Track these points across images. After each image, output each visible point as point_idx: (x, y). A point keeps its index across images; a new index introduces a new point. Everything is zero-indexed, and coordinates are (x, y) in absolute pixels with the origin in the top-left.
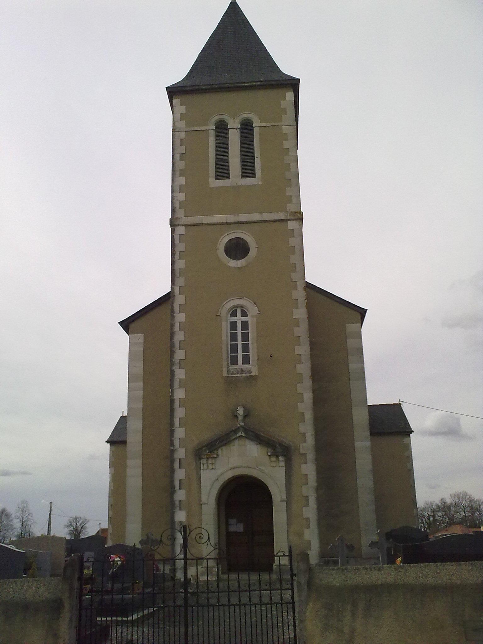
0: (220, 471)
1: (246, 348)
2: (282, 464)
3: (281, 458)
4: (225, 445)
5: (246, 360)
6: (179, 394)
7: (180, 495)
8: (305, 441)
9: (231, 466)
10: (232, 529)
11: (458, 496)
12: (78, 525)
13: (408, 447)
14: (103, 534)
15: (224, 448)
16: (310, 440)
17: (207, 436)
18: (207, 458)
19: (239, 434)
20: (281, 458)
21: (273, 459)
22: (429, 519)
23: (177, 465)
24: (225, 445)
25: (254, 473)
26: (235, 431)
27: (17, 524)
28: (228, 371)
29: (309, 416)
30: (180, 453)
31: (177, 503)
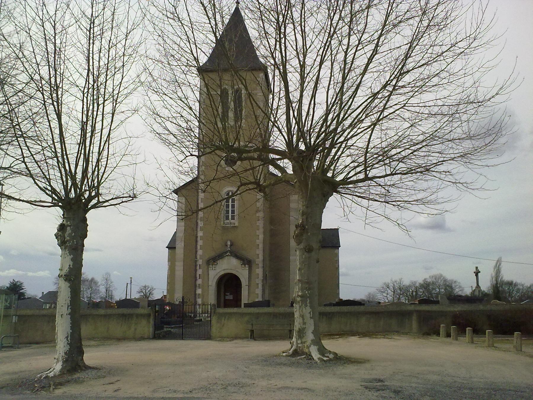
0: (218, 271)
1: (233, 212)
2: (247, 268)
3: (247, 266)
4: (221, 259)
5: (233, 218)
6: (200, 234)
7: (199, 282)
8: (258, 258)
9: (223, 269)
10: (227, 298)
11: (435, 277)
12: (147, 292)
13: (337, 255)
14: (297, 325)
15: (220, 260)
16: (261, 257)
17: (212, 254)
18: (212, 265)
19: (228, 254)
20: (247, 266)
21: (243, 266)
22: (412, 294)
23: (198, 267)
24: (221, 259)
25: (234, 272)
26: (226, 252)
27: (102, 289)
28: (224, 223)
29: (261, 246)
30: (200, 262)
31: (198, 285)
